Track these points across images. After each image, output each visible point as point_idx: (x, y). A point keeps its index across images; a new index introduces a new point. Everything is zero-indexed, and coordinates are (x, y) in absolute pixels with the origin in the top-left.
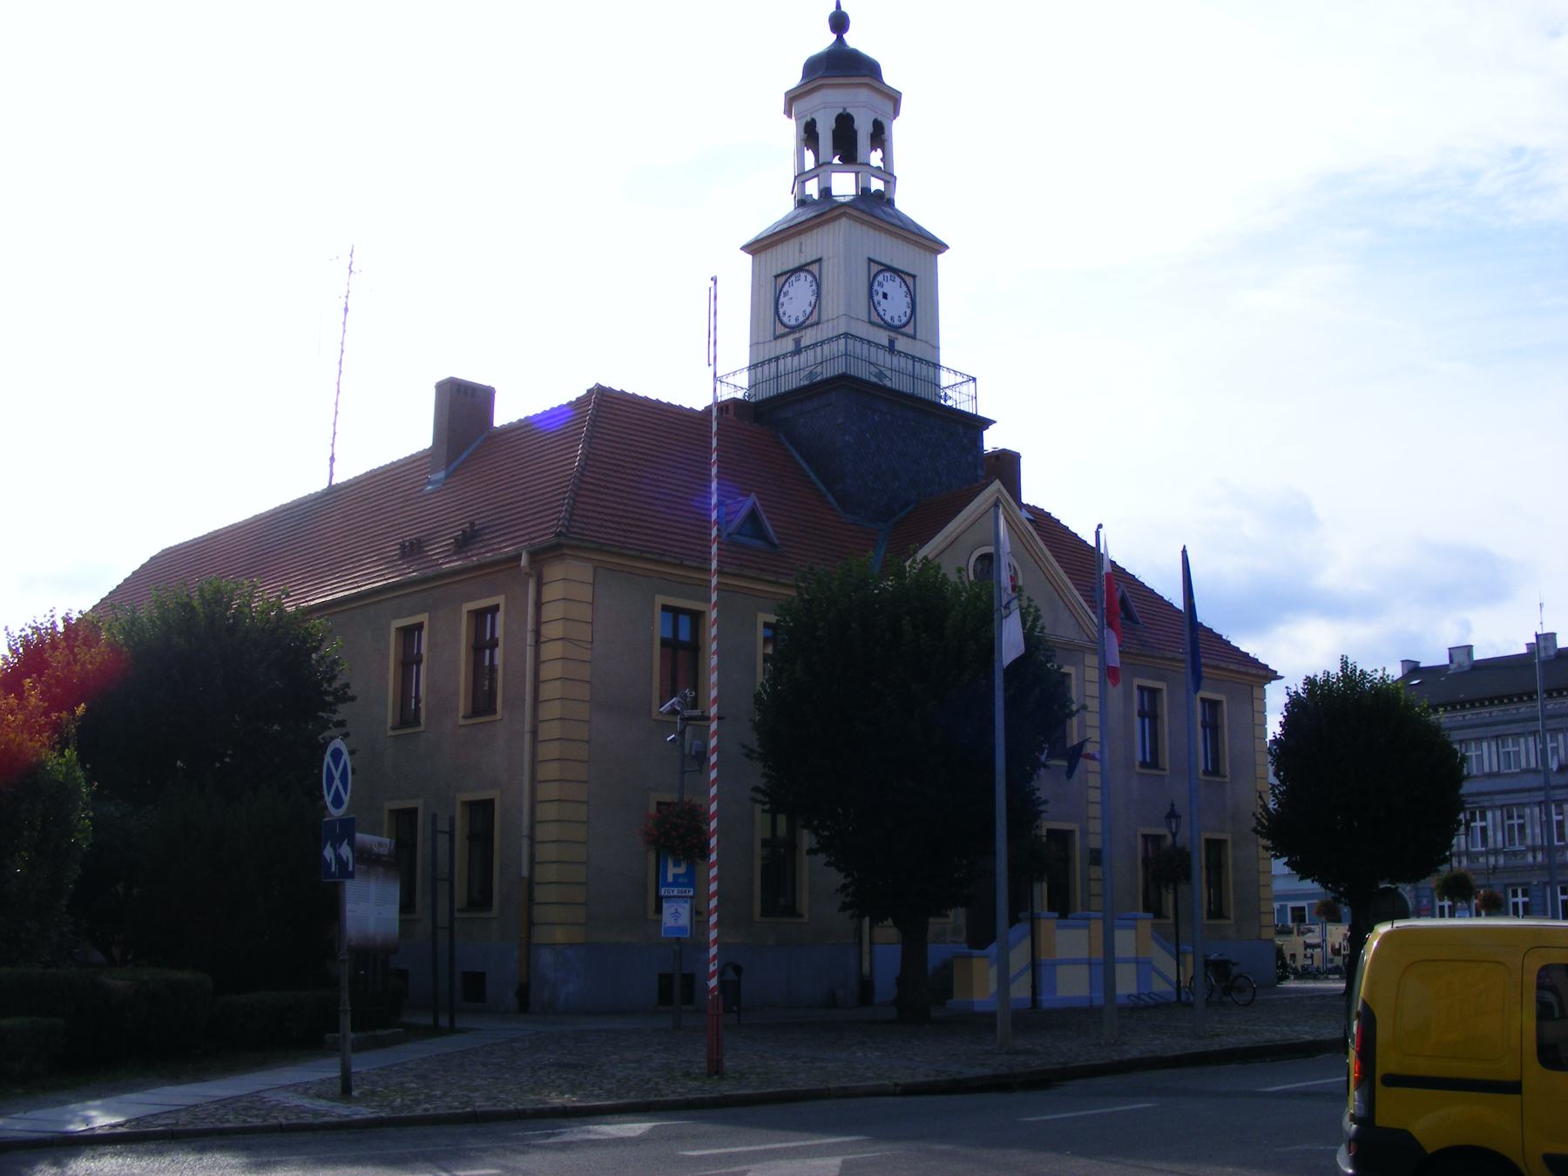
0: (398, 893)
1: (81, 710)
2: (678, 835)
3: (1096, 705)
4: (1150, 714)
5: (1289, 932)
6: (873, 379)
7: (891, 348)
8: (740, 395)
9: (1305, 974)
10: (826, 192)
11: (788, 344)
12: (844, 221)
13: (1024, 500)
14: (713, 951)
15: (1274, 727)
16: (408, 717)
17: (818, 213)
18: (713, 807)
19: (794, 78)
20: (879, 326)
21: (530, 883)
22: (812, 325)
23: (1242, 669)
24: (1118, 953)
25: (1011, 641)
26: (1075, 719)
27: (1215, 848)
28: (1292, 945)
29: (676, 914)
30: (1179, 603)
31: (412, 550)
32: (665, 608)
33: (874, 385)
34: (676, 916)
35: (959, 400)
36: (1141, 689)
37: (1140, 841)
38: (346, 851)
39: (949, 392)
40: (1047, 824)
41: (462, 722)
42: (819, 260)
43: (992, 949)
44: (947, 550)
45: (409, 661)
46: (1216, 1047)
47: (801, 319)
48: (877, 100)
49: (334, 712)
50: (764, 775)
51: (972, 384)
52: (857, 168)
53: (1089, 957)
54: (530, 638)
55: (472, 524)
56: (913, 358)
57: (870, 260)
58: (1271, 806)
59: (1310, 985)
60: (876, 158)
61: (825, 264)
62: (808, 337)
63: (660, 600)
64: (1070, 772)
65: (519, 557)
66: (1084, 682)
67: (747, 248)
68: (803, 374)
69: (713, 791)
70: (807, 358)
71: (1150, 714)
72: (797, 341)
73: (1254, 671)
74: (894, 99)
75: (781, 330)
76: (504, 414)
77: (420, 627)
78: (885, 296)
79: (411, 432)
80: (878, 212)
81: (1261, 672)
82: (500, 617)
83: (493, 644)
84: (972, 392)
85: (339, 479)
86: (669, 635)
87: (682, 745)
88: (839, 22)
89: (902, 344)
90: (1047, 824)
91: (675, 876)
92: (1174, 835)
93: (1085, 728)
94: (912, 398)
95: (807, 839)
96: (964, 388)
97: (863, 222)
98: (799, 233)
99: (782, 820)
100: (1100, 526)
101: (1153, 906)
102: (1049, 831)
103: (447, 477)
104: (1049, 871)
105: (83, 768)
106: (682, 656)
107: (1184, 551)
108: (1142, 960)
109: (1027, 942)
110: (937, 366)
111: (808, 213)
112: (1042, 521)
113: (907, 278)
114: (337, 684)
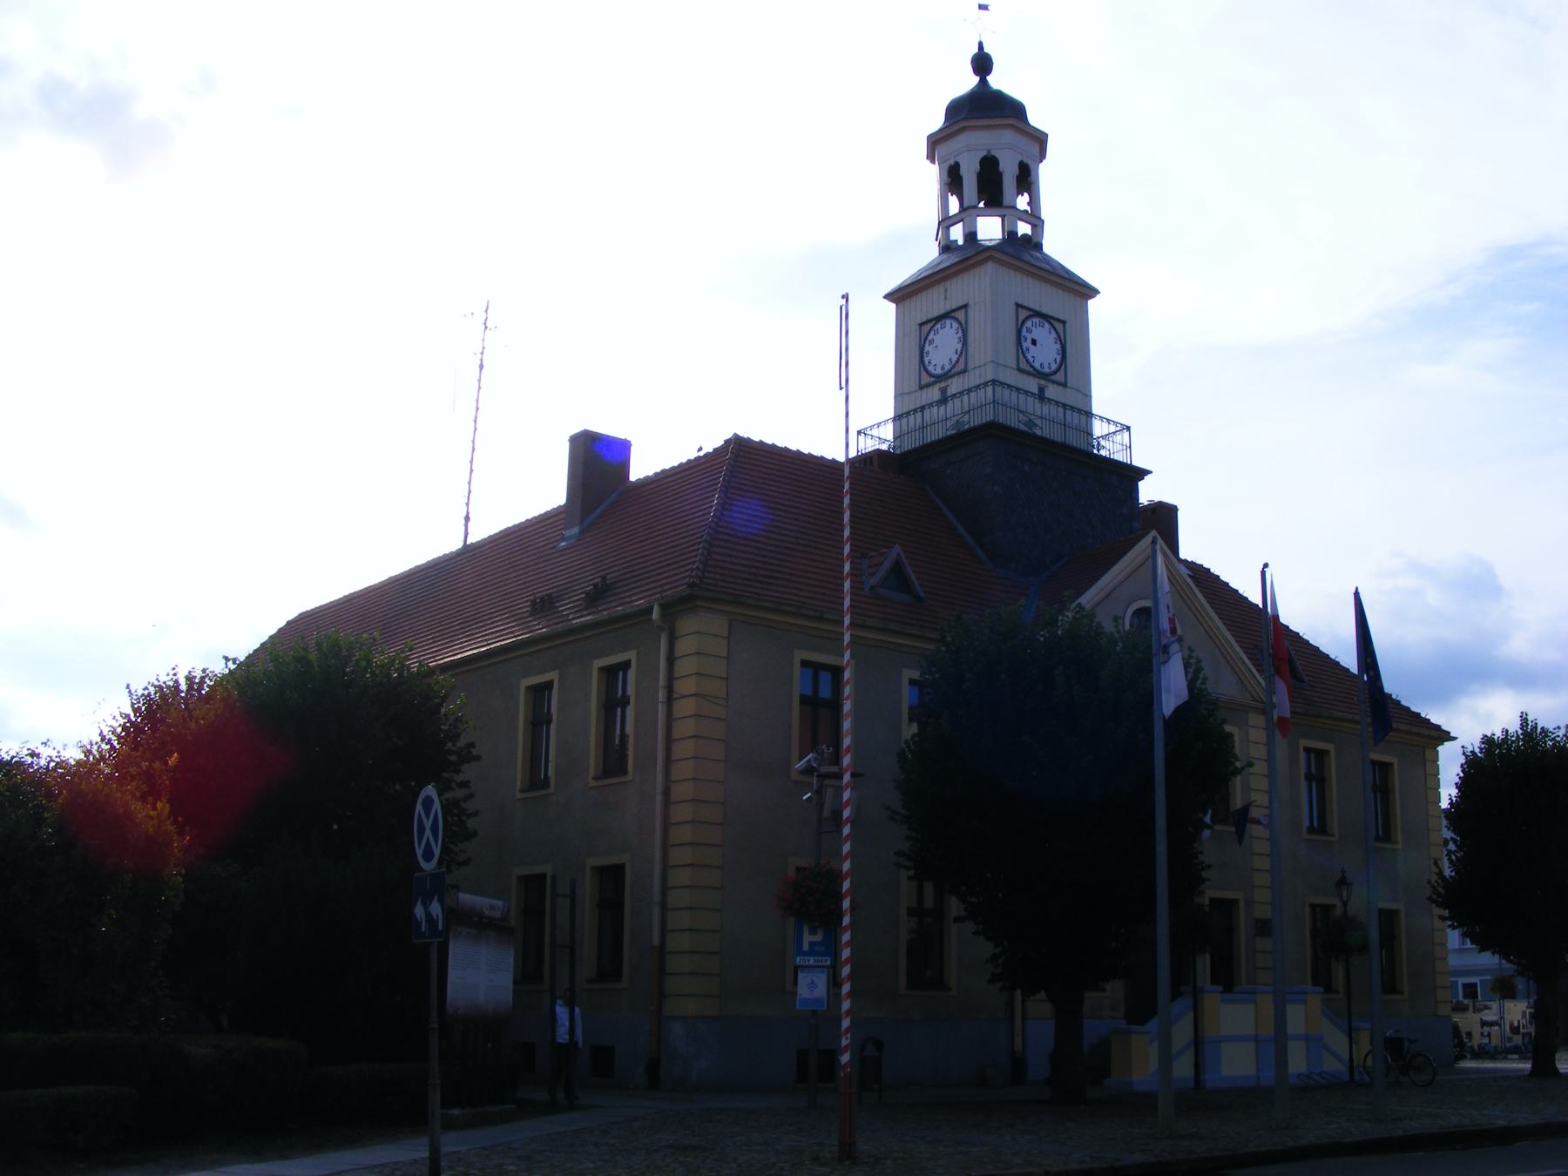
0: (511, 960)
1: (173, 760)
2: (812, 900)
3: (1262, 765)
4: (1317, 778)
5: (1464, 1009)
6: (1022, 427)
7: (1041, 396)
8: (884, 447)
9: (1482, 1053)
10: (971, 236)
11: (934, 394)
12: (990, 266)
13: (1182, 556)
14: (846, 1023)
15: (1447, 793)
16: (536, 781)
17: (962, 258)
18: (846, 866)
19: (937, 121)
20: (1029, 373)
21: (662, 951)
22: (959, 373)
23: (1415, 730)
24: (1290, 1030)
25: (1173, 687)
26: (1239, 777)
27: (1388, 918)
28: (1469, 1022)
29: (812, 985)
30: (1348, 658)
31: (543, 606)
32: (804, 663)
33: (1023, 432)
34: (811, 987)
35: (1112, 449)
36: (1308, 750)
37: (1308, 910)
38: (436, 908)
39: (1103, 443)
40: (1210, 893)
41: (593, 783)
42: (965, 306)
43: (1153, 1025)
44: (1105, 598)
45: (539, 722)
46: (1400, 1132)
47: (947, 367)
48: (1023, 142)
49: (458, 772)
50: (908, 838)
51: (1126, 434)
52: (1003, 212)
53: (1245, 1034)
54: (662, 695)
55: (604, 578)
56: (1064, 406)
57: (1018, 305)
58: (1448, 872)
59: (1489, 1065)
60: (1022, 202)
62: (954, 386)
63: (799, 655)
64: (1240, 834)
65: (650, 611)
66: (1250, 740)
67: (889, 297)
68: (949, 423)
69: (846, 848)
70: (953, 407)
71: (1317, 778)
72: (943, 391)
73: (1426, 732)
74: (1039, 140)
75: (926, 379)
76: (639, 469)
77: (549, 685)
78: (1034, 342)
79: (543, 488)
80: (1026, 256)
81: (1433, 733)
82: (632, 674)
83: (625, 702)
84: (1126, 441)
85: (473, 539)
86: (809, 692)
87: (821, 805)
88: (982, 64)
89: (1052, 392)
90: (1210, 893)
91: (812, 944)
92: (1345, 904)
93: (1251, 788)
94: (1063, 447)
95: (955, 907)
96: (1118, 438)
97: (1010, 266)
98: (945, 279)
99: (929, 888)
100: (1266, 565)
101: (1322, 979)
102: (1211, 900)
103: (582, 532)
104: (1212, 944)
105: (175, 822)
106: (820, 713)
107: (1357, 594)
108: (1316, 1038)
109: (1190, 1017)
110: (1089, 415)
111: (952, 259)
112: (1201, 576)
113: (1057, 325)
114: (461, 743)
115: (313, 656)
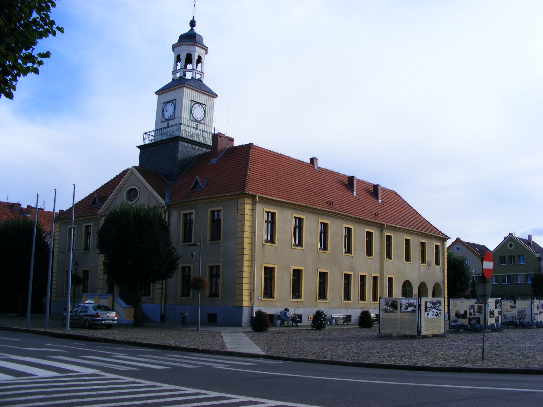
6: (189, 138)
11: (165, 125)
19: (176, 40)
36: (346, 228)
42: (175, 99)
61: (177, 101)
62: (171, 123)
72: (168, 124)
75: (164, 120)
88: (193, 24)
89: (201, 127)
115: (142, 214)
